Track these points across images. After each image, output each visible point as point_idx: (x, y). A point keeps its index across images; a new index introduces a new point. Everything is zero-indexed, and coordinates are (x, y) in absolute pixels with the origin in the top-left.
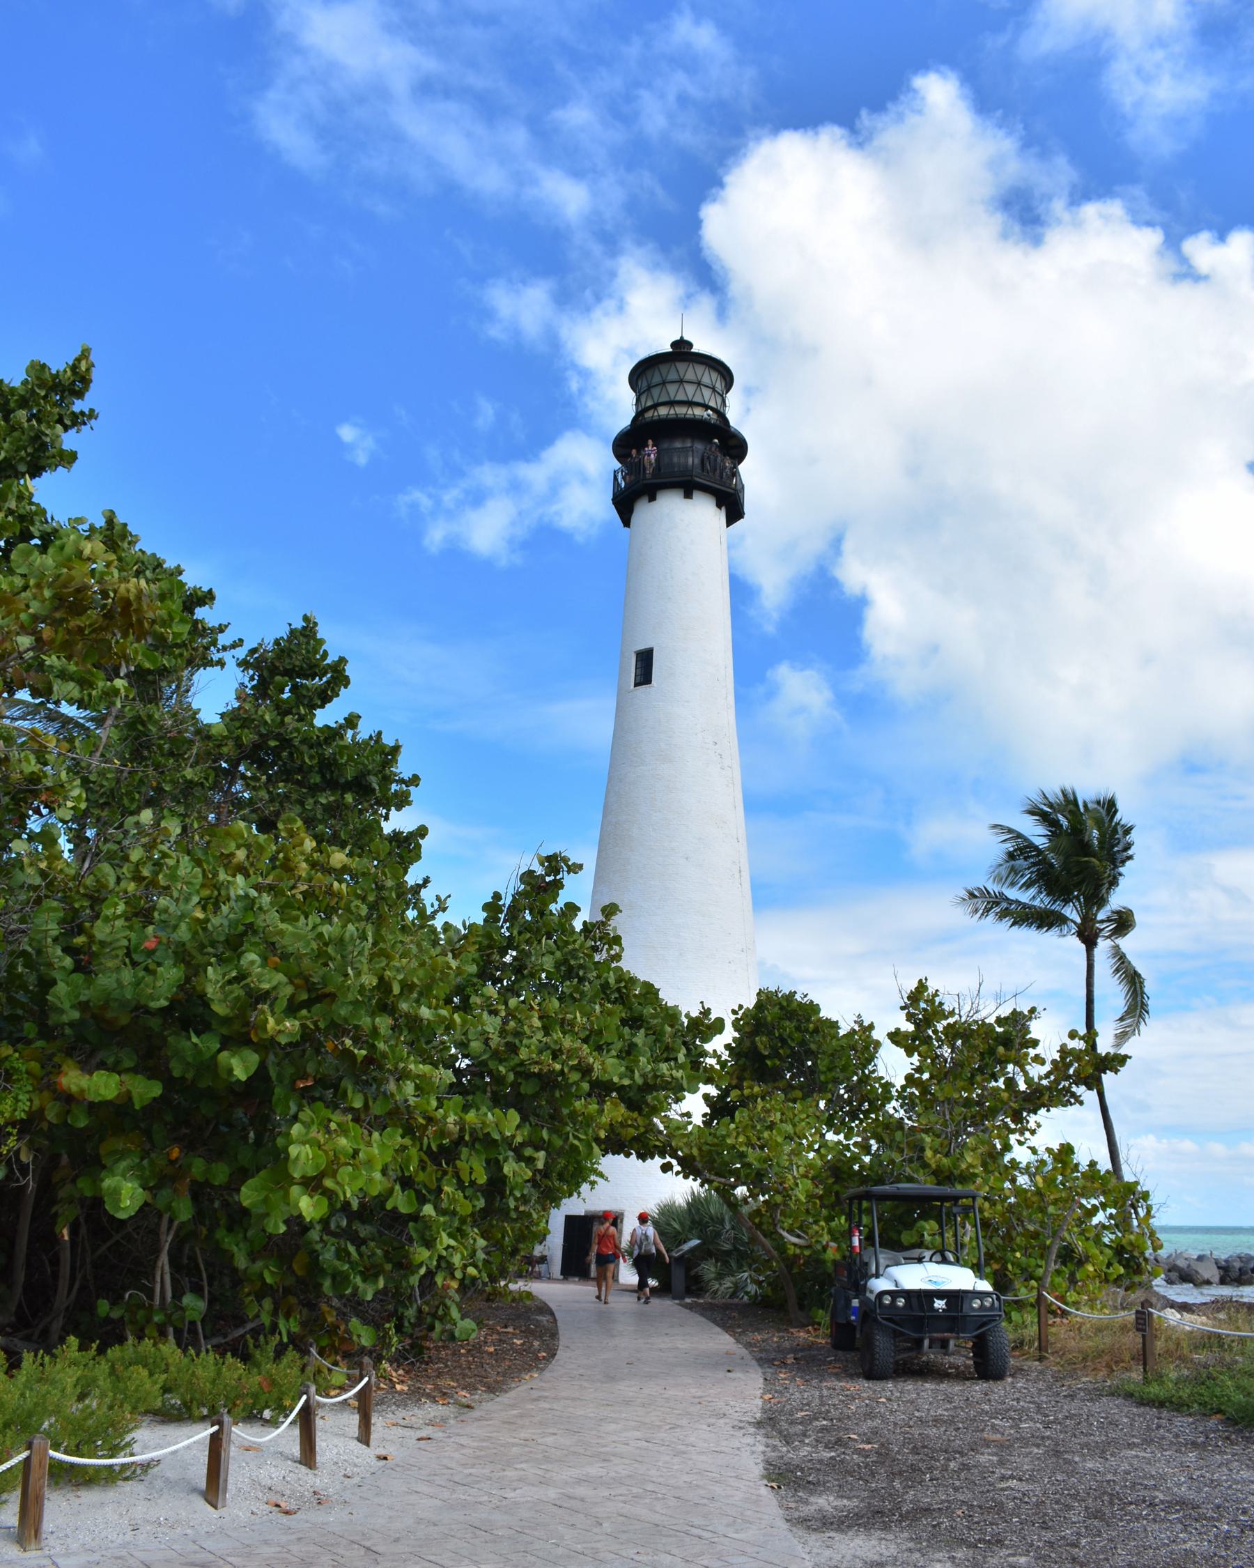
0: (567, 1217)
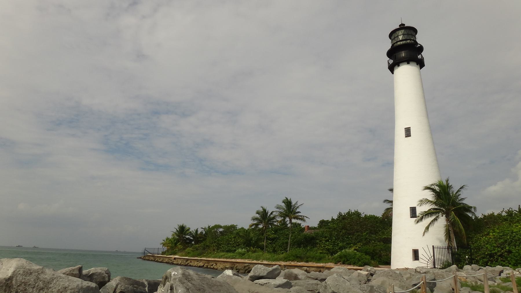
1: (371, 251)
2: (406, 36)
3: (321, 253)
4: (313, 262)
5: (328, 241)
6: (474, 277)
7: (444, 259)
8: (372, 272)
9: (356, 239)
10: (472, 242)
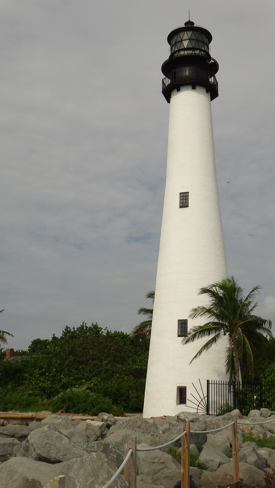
0: (179, 320)
1: (114, 390)
2: (194, 43)
3: (30, 395)
4: (16, 410)
5: (44, 374)
6: (261, 425)
7: (222, 402)
8: (109, 423)
9: (90, 371)
10: (264, 375)
